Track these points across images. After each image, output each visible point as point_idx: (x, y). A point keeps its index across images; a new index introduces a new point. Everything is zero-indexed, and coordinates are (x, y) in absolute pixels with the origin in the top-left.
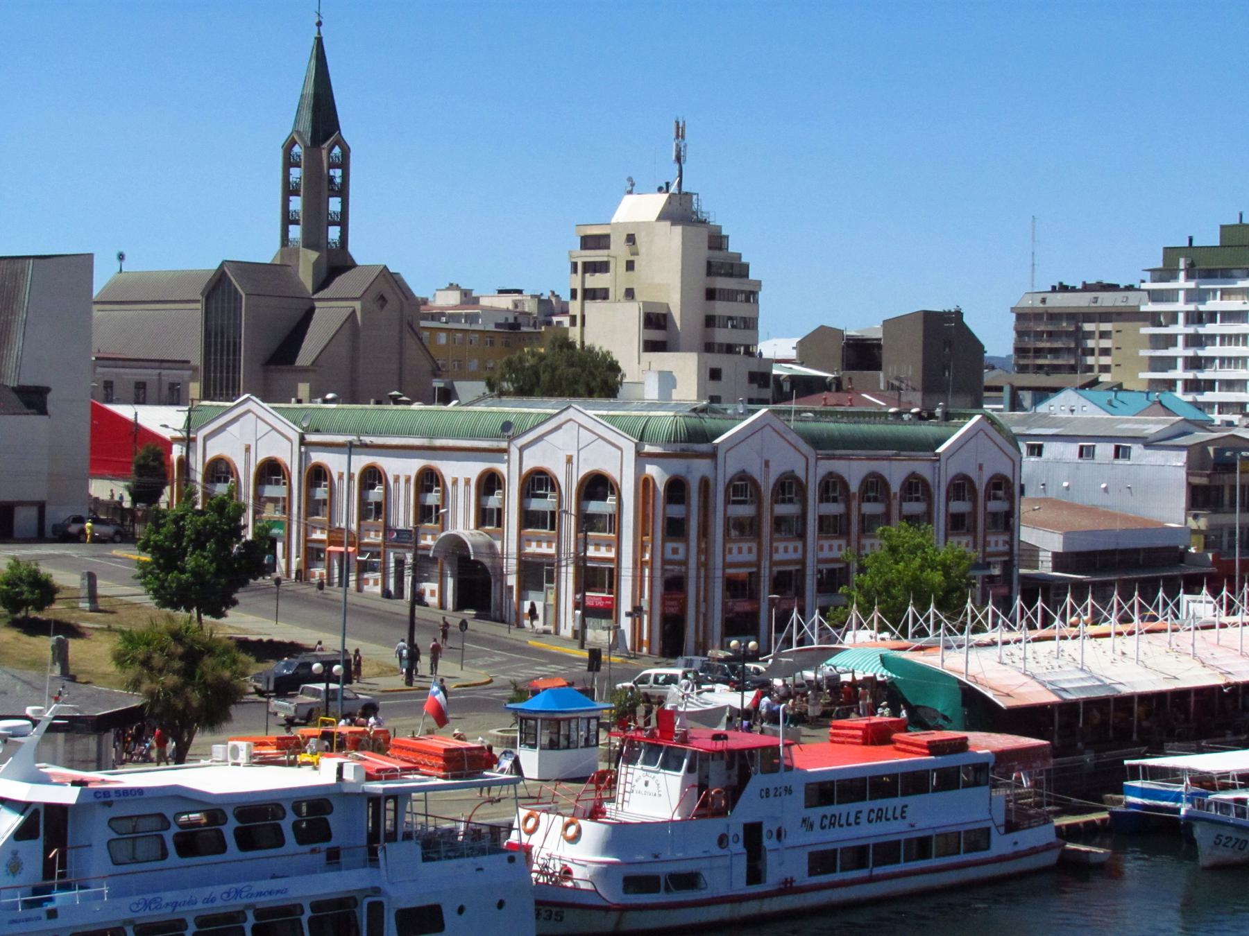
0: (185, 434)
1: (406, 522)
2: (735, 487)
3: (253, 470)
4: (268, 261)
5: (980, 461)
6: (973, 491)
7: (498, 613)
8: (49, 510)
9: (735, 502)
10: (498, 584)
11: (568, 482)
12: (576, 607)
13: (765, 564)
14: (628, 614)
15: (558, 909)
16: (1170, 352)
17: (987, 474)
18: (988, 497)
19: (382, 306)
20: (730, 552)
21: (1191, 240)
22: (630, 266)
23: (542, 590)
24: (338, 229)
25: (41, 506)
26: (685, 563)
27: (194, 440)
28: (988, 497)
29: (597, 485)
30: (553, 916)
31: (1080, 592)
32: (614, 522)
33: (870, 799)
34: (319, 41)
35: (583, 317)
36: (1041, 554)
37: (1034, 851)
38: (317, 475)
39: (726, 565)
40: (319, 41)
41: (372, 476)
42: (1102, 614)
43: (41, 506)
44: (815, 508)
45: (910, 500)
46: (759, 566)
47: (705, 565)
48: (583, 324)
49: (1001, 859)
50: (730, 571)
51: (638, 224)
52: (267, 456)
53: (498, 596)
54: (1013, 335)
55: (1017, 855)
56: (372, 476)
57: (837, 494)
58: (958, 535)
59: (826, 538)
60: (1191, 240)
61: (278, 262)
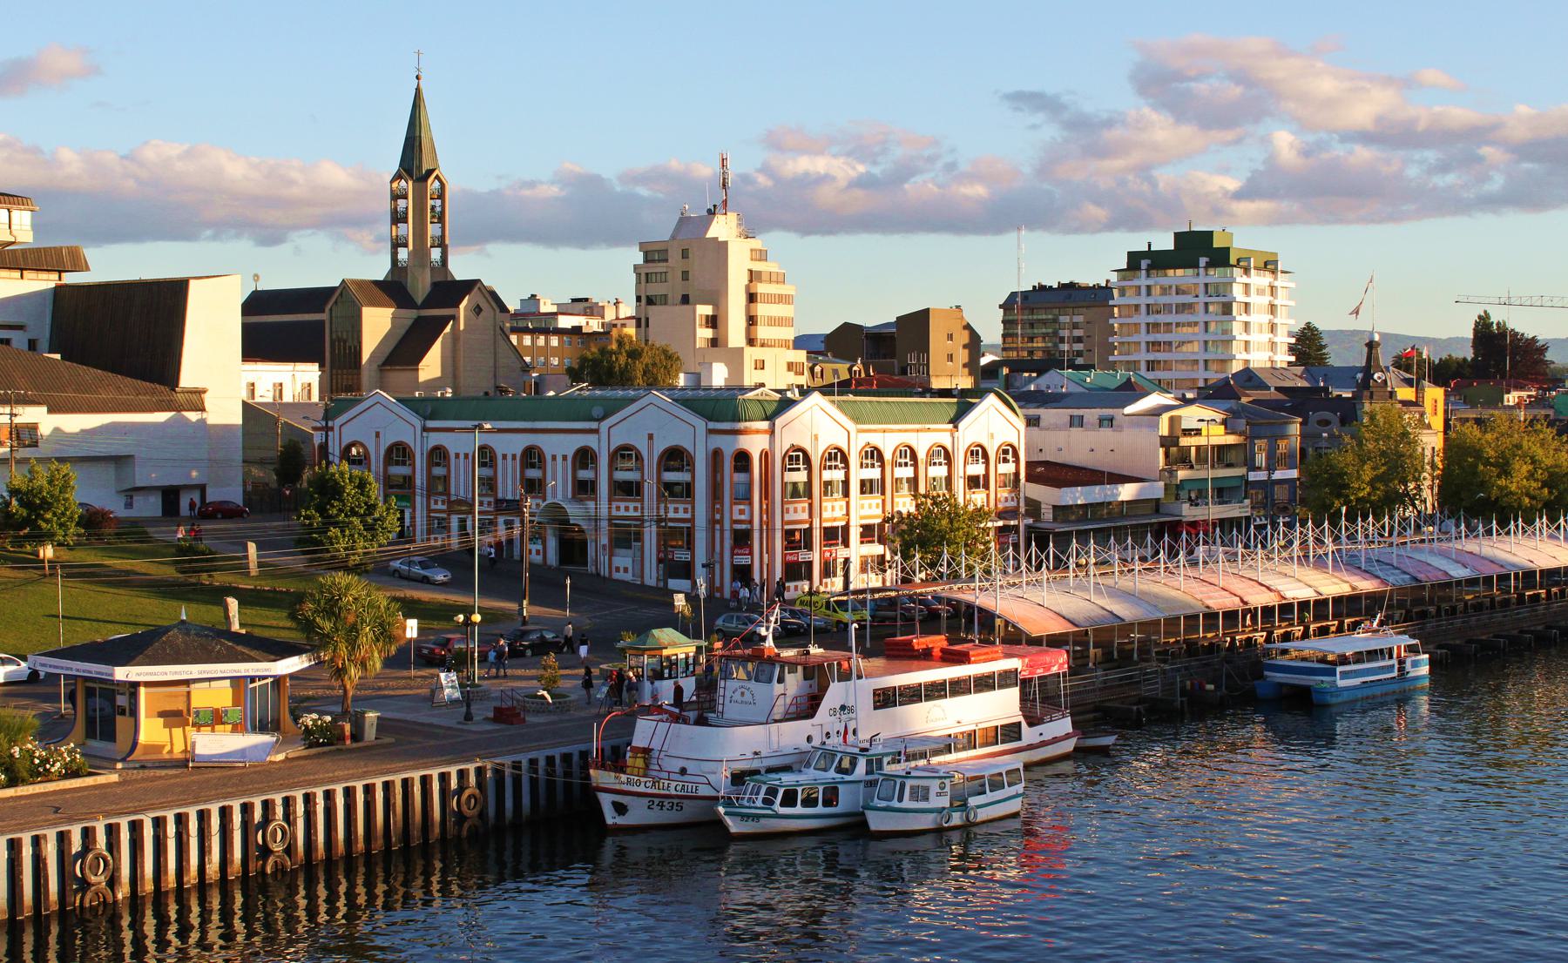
0: (324, 423)
1: (514, 493)
2: (791, 458)
3: (382, 453)
4: (381, 279)
5: (991, 431)
6: (986, 456)
7: (594, 568)
8: (209, 491)
9: (790, 470)
10: (594, 544)
11: (651, 455)
12: (660, 561)
13: (816, 523)
14: (703, 566)
15: (678, 801)
16: (1135, 338)
17: (660, 446)
18: (895, 464)
19: (478, 314)
20: (788, 512)
21: (1150, 246)
22: (685, 276)
23: (630, 548)
24: (439, 250)
25: (202, 488)
26: (751, 522)
27: (332, 429)
28: (998, 461)
29: (675, 457)
30: (675, 807)
31: (1083, 537)
32: (687, 491)
33: (975, 692)
34: (418, 90)
35: (647, 319)
36: (1043, 506)
37: (1055, 740)
38: (438, 455)
39: (783, 523)
40: (418, 90)
41: (532, 457)
42: (484, 592)
43: (202, 488)
44: (858, 474)
45: (830, 467)
46: (811, 523)
47: (713, 523)
48: (647, 325)
49: (1031, 747)
50: (787, 527)
51: (1419, 338)
52: (681, 444)
53: (594, 554)
54: (781, 305)
55: (1043, 744)
56: (532, 457)
57: (908, 460)
58: (677, 502)
59: (866, 498)
60: (1150, 246)
61: (389, 279)
